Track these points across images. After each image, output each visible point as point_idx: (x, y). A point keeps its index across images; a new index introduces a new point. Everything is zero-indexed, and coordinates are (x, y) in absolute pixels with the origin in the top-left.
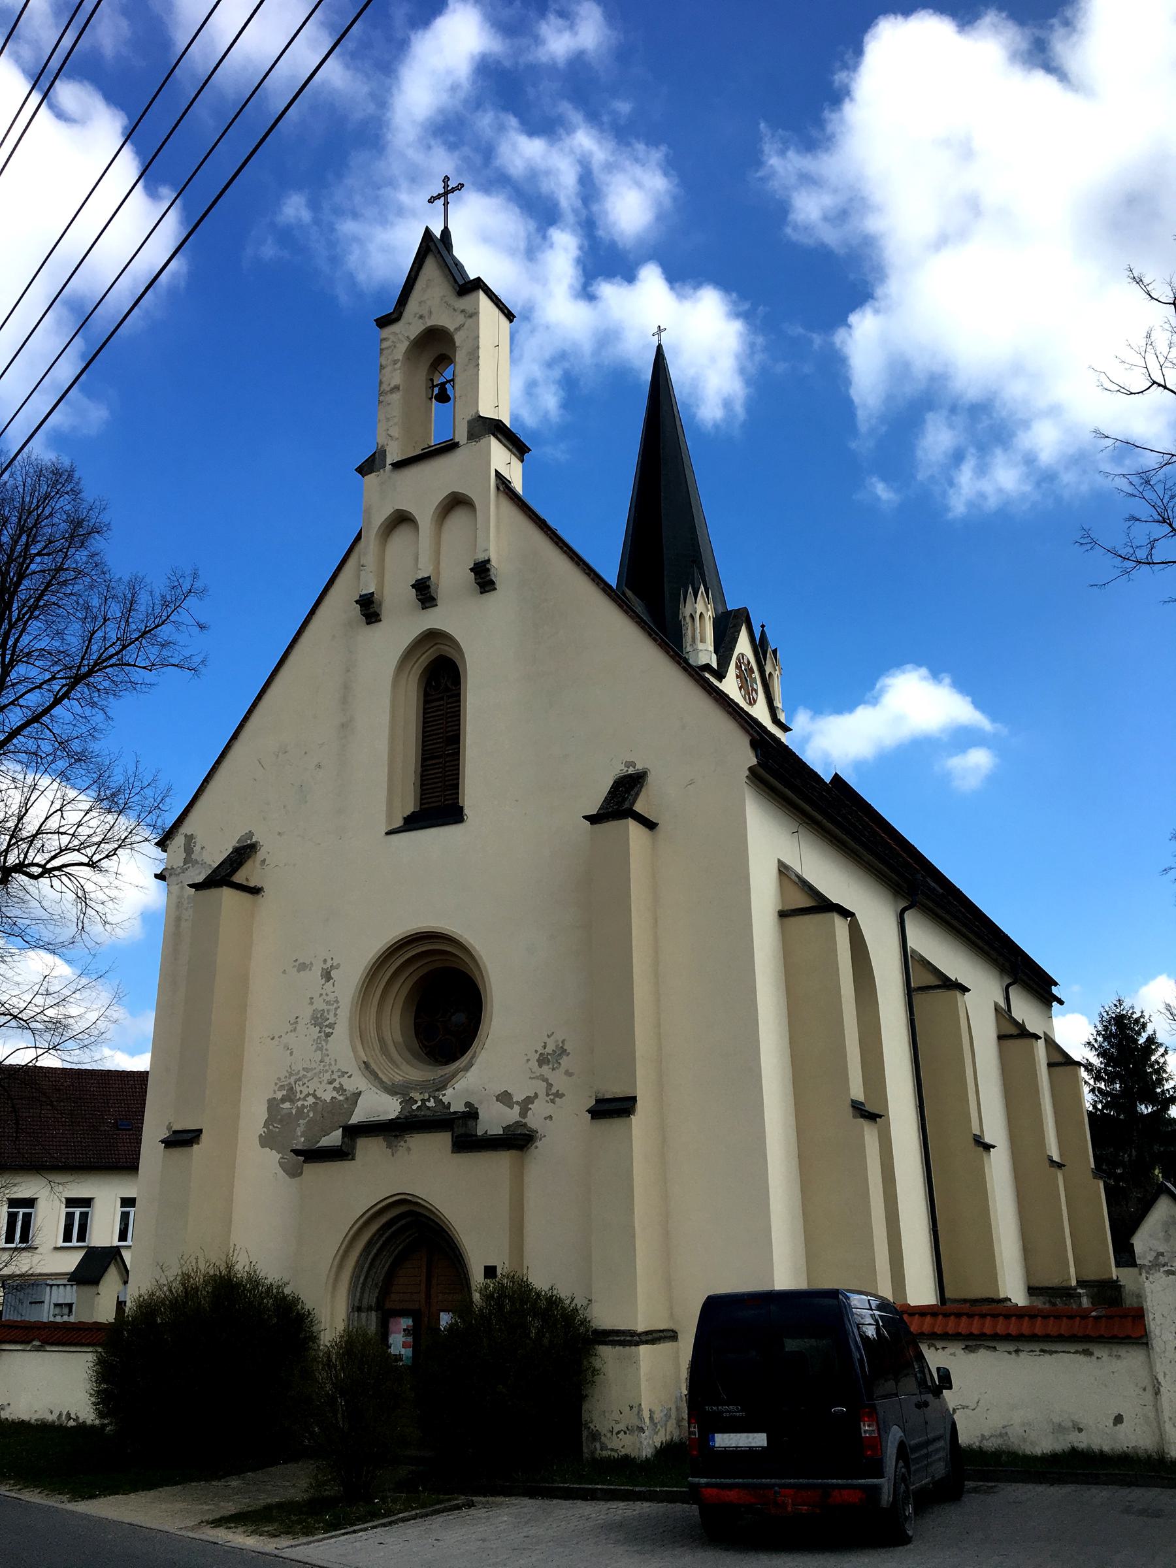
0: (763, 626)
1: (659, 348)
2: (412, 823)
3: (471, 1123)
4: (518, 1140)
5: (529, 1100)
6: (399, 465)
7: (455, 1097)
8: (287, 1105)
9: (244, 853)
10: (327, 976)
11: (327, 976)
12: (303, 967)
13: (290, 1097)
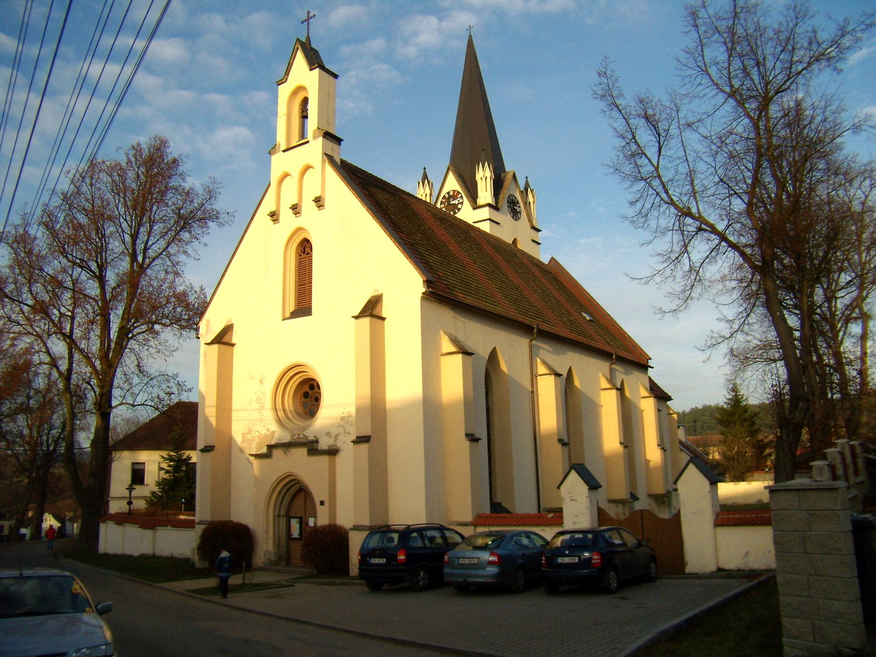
0: (720, 367)
1: (470, 36)
2: (295, 315)
3: (315, 445)
4: (333, 452)
5: (337, 435)
6: (284, 151)
7: (310, 434)
8: (248, 436)
9: (228, 329)
10: (261, 382)
11: (261, 382)
12: (252, 378)
13: (249, 432)
